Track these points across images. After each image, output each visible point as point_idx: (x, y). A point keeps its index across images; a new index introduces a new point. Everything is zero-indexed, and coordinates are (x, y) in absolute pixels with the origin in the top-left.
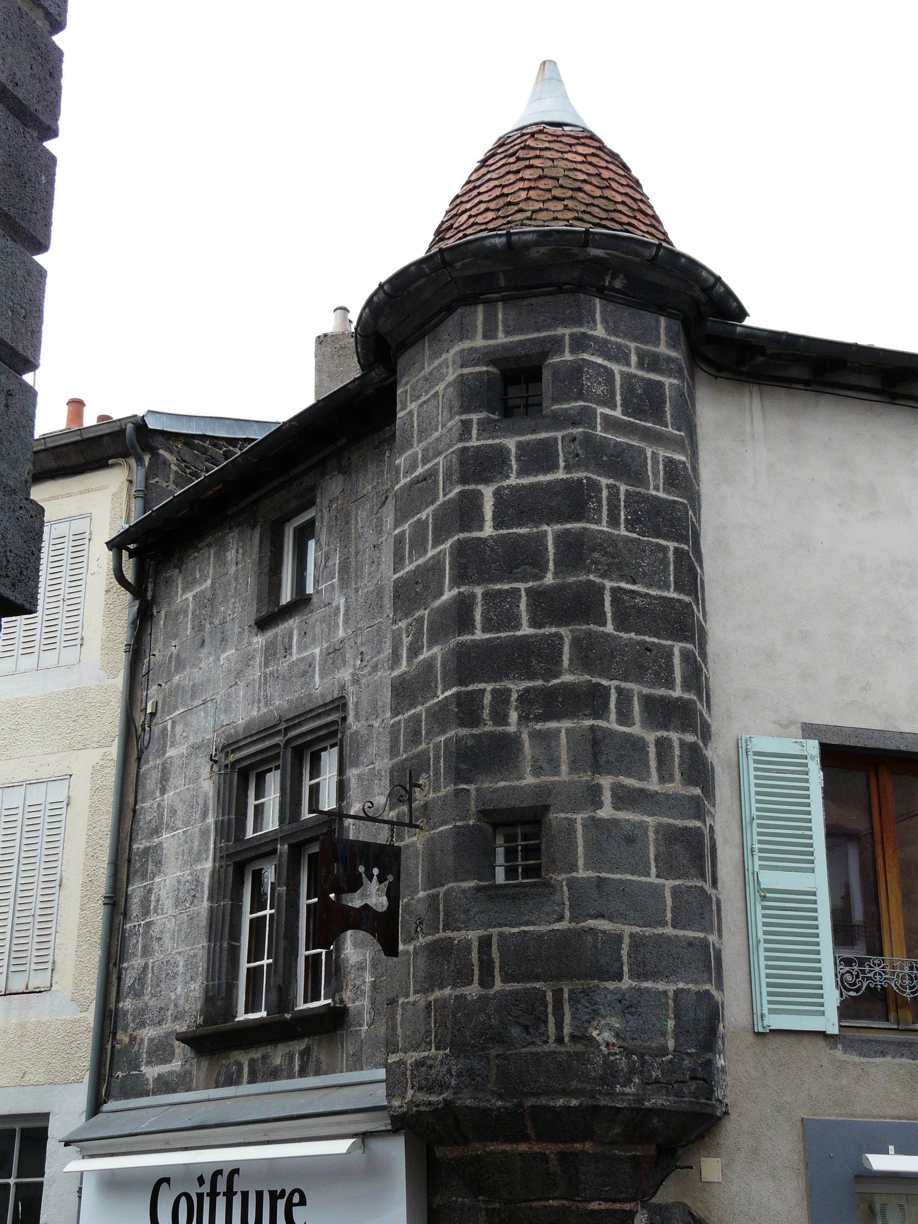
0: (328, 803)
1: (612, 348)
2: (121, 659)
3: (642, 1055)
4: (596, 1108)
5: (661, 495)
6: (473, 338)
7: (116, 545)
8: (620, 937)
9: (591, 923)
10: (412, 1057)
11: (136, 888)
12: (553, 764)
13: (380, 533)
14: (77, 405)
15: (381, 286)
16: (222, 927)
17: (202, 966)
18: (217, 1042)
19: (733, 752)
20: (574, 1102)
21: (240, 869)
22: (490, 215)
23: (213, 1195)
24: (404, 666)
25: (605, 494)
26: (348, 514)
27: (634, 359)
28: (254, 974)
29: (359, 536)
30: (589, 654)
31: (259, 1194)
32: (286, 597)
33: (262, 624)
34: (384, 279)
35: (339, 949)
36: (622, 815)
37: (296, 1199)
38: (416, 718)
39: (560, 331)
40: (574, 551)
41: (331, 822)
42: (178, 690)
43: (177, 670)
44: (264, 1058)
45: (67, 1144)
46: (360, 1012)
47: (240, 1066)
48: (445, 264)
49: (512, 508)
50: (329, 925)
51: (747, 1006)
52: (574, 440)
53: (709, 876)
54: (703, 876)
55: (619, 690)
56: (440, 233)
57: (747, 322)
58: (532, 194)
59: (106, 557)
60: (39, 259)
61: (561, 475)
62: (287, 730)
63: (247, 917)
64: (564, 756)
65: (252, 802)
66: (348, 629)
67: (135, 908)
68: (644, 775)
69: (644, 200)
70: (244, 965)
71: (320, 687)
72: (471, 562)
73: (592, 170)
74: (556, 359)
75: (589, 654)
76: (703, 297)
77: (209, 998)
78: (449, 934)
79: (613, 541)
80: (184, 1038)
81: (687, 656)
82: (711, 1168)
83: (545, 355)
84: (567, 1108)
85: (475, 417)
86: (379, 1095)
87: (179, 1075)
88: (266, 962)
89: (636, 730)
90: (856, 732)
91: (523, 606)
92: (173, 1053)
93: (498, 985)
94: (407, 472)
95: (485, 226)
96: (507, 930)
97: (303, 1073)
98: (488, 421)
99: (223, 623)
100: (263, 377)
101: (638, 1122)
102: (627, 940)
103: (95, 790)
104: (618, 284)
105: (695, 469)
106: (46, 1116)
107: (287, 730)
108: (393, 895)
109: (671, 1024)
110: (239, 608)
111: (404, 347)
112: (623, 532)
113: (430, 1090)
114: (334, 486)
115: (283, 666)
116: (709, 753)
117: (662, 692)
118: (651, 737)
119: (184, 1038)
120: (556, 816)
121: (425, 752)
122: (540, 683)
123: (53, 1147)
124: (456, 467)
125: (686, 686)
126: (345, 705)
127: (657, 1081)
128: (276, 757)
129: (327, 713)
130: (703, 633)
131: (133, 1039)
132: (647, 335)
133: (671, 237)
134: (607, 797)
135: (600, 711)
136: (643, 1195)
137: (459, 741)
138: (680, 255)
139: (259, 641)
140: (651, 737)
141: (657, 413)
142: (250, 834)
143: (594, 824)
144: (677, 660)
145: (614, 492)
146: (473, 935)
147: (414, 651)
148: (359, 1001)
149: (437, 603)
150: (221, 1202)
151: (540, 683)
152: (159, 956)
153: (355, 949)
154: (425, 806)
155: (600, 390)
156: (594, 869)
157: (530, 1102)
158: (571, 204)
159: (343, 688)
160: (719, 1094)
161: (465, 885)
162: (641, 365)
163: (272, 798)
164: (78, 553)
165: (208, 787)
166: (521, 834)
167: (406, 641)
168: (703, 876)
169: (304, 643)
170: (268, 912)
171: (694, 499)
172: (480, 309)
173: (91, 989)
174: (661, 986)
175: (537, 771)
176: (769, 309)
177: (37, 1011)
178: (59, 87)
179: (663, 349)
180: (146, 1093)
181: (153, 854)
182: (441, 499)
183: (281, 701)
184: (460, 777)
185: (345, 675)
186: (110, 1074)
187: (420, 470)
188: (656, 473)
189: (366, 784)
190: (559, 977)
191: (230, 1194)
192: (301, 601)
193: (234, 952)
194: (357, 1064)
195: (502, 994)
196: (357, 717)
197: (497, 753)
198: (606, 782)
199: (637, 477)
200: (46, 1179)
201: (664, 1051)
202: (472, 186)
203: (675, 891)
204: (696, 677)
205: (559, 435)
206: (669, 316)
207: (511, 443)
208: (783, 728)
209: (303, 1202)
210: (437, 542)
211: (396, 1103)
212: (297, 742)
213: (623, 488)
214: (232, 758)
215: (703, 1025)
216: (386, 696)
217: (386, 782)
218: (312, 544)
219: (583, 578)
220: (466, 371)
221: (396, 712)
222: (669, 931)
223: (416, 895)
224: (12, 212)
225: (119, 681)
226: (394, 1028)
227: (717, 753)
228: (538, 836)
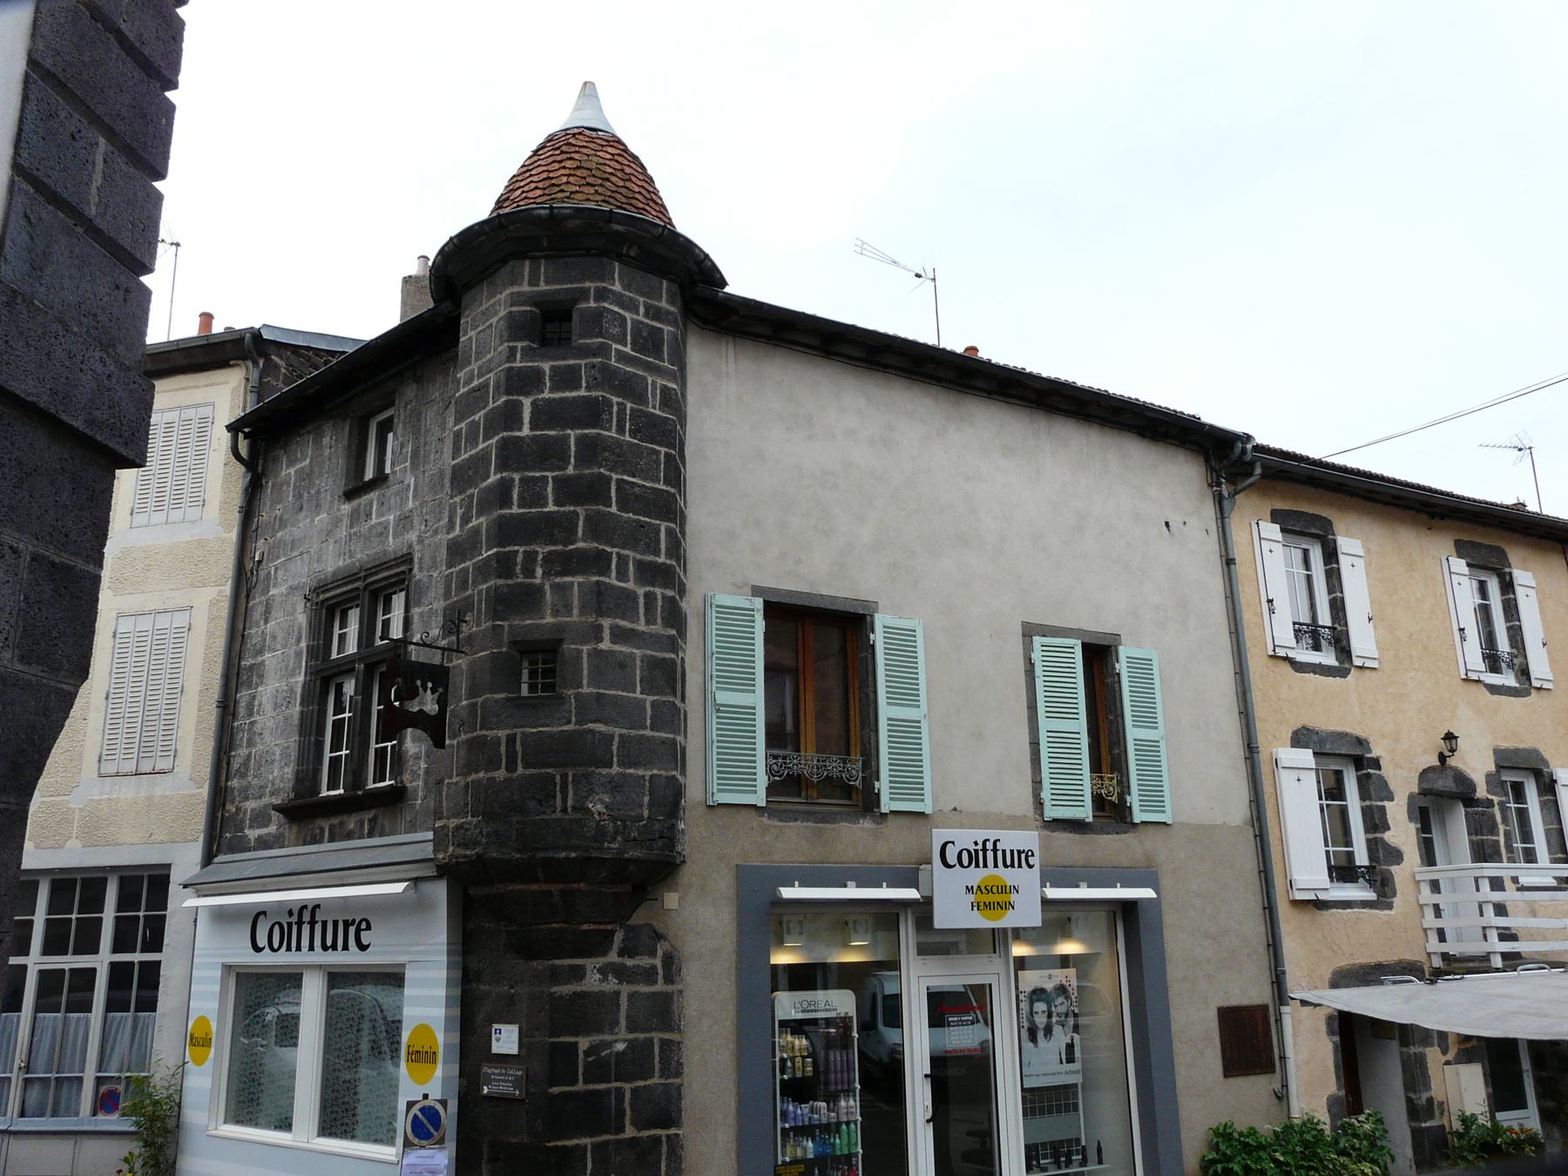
0: (396, 632)
1: (625, 302)
2: (235, 518)
3: (624, 821)
4: (589, 859)
5: (657, 412)
6: (521, 284)
7: (233, 428)
8: (612, 737)
9: (591, 726)
10: (453, 823)
11: (243, 696)
12: (568, 609)
13: (444, 429)
14: (207, 318)
15: (451, 239)
16: (310, 726)
17: (294, 755)
18: (305, 812)
19: (701, 604)
20: (573, 855)
21: (326, 682)
22: (539, 192)
23: (300, 923)
24: (457, 531)
25: (615, 409)
26: (420, 413)
27: (642, 310)
28: (335, 762)
29: (427, 431)
30: (598, 528)
31: (335, 923)
32: (369, 474)
33: (349, 495)
34: (453, 234)
35: (401, 743)
36: (617, 648)
37: (364, 926)
38: (465, 570)
39: (587, 284)
40: (590, 450)
41: (395, 648)
42: (280, 545)
43: (280, 529)
44: (341, 823)
45: (185, 886)
46: (416, 790)
47: (322, 830)
48: (501, 226)
49: (546, 415)
50: (393, 725)
51: (702, 787)
52: (594, 367)
53: (679, 694)
54: (675, 694)
55: (618, 555)
56: (500, 203)
57: (727, 290)
58: (571, 179)
59: (225, 438)
60: (157, 185)
61: (583, 393)
62: (366, 577)
63: (330, 718)
64: (576, 603)
65: (337, 632)
66: (414, 502)
67: (242, 711)
68: (635, 619)
69: (656, 193)
70: (327, 755)
71: (393, 545)
72: (511, 455)
73: (618, 166)
74: (584, 305)
75: (598, 528)
76: (694, 267)
77: (299, 778)
78: (484, 732)
79: (619, 444)
80: (277, 808)
81: (670, 532)
82: (671, 900)
83: (575, 301)
84: (567, 858)
85: (519, 345)
86: (428, 851)
87: (274, 836)
88: (344, 752)
89: (630, 585)
90: (790, 593)
91: (550, 490)
92: (270, 820)
93: (520, 770)
94: (466, 383)
95: (534, 200)
96: (528, 730)
97: (370, 835)
98: (530, 348)
99: (318, 492)
100: (361, 305)
101: (619, 868)
102: (617, 739)
103: (211, 619)
104: (633, 253)
105: (684, 396)
106: (169, 866)
107: (366, 577)
108: (442, 703)
109: (646, 799)
110: (330, 482)
111: (468, 287)
112: (628, 438)
113: (466, 846)
114: (410, 391)
115: (364, 528)
116: (683, 605)
117: (651, 558)
118: (641, 591)
119: (277, 808)
120: (568, 647)
121: (471, 596)
122: (560, 547)
123: (174, 889)
124: (503, 381)
125: (669, 555)
126: (411, 560)
127: (634, 839)
128: (357, 597)
129: (398, 565)
130: (683, 517)
131: (238, 809)
132: (653, 293)
133: (675, 222)
134: (606, 634)
135: (605, 571)
136: (621, 919)
137: (497, 588)
138: (679, 235)
139: (346, 508)
140: (641, 591)
141: (657, 351)
142: (334, 656)
143: (597, 654)
144: (663, 535)
145: (622, 407)
146: (502, 734)
147: (466, 519)
148: (415, 782)
149: (485, 484)
150: (306, 929)
151: (560, 547)
152: (260, 747)
153: (413, 743)
154: (470, 637)
155: (615, 331)
156: (595, 686)
157: (540, 855)
158: (600, 190)
159: (410, 546)
160: (679, 848)
161: (497, 696)
162: (647, 315)
163: (353, 629)
164: (202, 434)
165: (302, 619)
166: (542, 659)
167: (459, 512)
168: (675, 694)
169: (382, 511)
170: (347, 715)
171: (682, 417)
172: (527, 263)
173: (206, 771)
174: (640, 772)
175: (555, 613)
176: (746, 279)
177: (162, 788)
178: (181, 50)
179: (664, 304)
180: (244, 850)
181: (258, 671)
182: (491, 406)
183: (362, 555)
184: (497, 615)
185: (412, 536)
186: (221, 832)
187: (476, 383)
188: (654, 396)
189: (426, 622)
190: (566, 765)
191: (312, 923)
192: (381, 479)
193: (319, 745)
194: (412, 828)
195: (523, 777)
196: (421, 569)
197: (528, 598)
198: (606, 623)
199: (640, 397)
200: (168, 913)
201: (641, 818)
202: (526, 169)
203: (653, 704)
204: (676, 547)
205: (583, 362)
206: (669, 280)
207: (546, 366)
208: (738, 588)
209: (369, 928)
210: (487, 437)
211: (440, 856)
212: (373, 586)
213: (629, 405)
214: (322, 597)
215: (670, 799)
216: (443, 554)
217: (440, 618)
218: (391, 435)
219: (596, 470)
220: (514, 309)
221: (449, 566)
222: (648, 732)
223: (461, 703)
224: (135, 145)
225: (234, 535)
226: (440, 802)
227: (689, 605)
228: (554, 661)
